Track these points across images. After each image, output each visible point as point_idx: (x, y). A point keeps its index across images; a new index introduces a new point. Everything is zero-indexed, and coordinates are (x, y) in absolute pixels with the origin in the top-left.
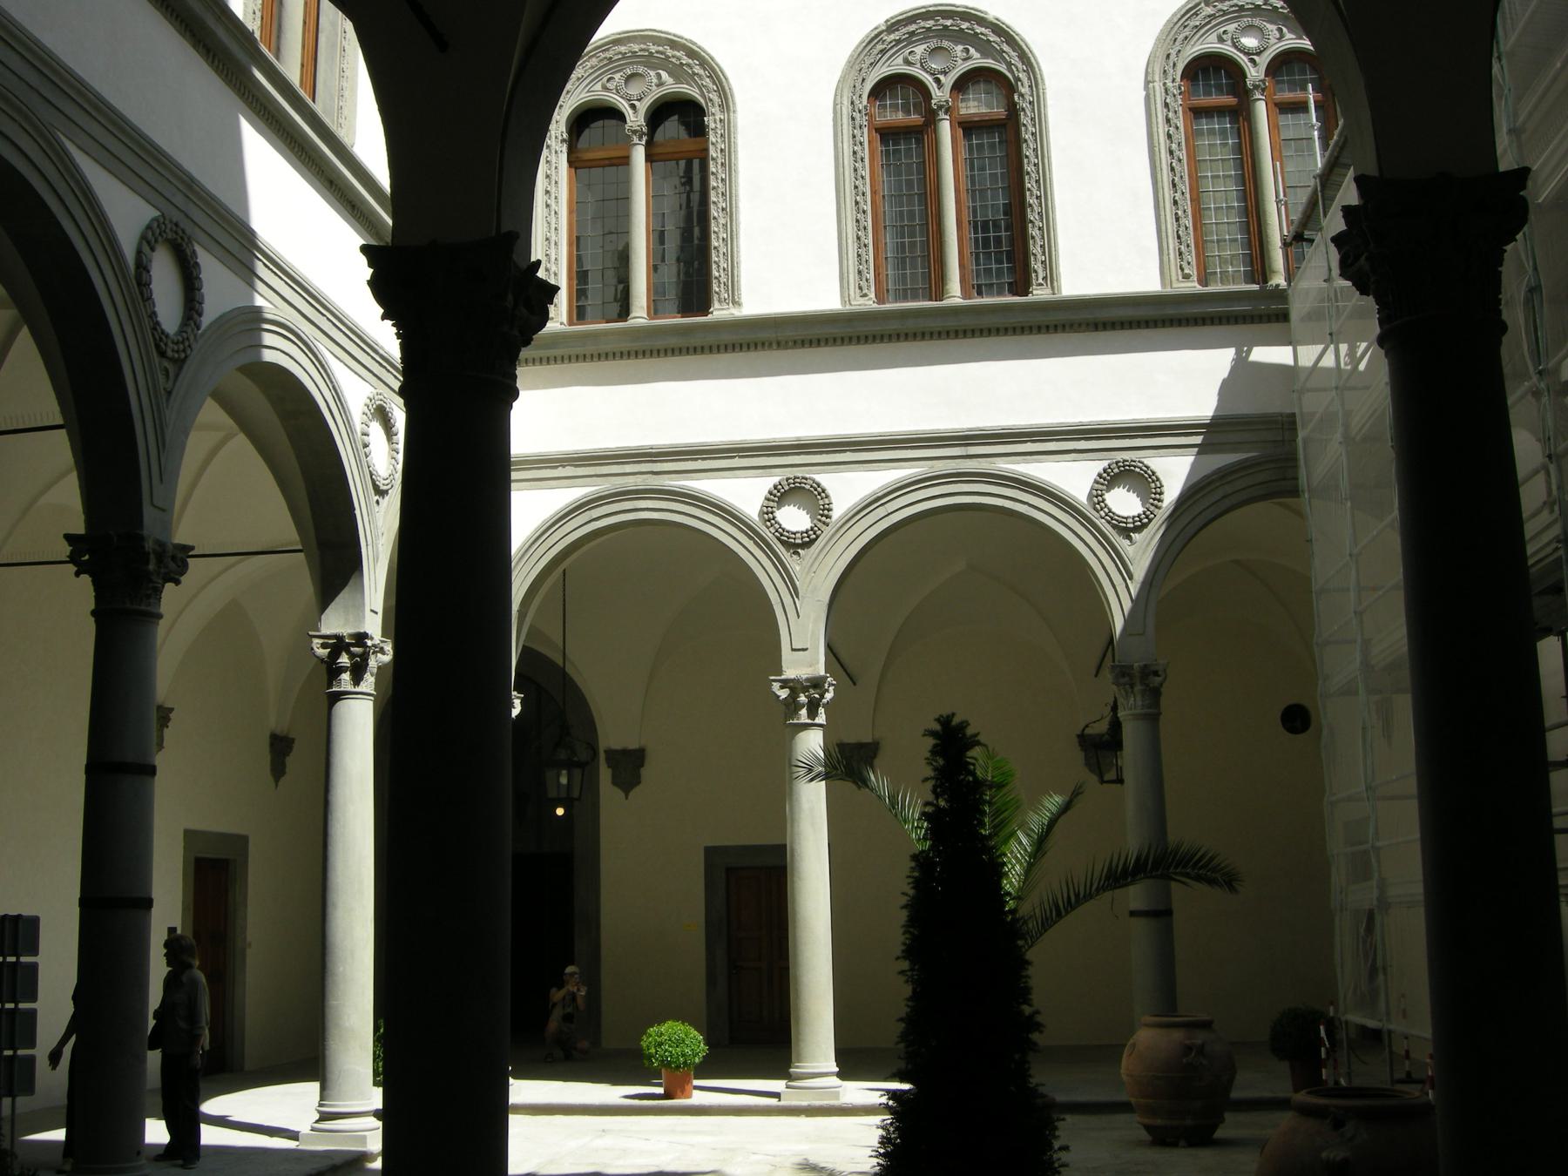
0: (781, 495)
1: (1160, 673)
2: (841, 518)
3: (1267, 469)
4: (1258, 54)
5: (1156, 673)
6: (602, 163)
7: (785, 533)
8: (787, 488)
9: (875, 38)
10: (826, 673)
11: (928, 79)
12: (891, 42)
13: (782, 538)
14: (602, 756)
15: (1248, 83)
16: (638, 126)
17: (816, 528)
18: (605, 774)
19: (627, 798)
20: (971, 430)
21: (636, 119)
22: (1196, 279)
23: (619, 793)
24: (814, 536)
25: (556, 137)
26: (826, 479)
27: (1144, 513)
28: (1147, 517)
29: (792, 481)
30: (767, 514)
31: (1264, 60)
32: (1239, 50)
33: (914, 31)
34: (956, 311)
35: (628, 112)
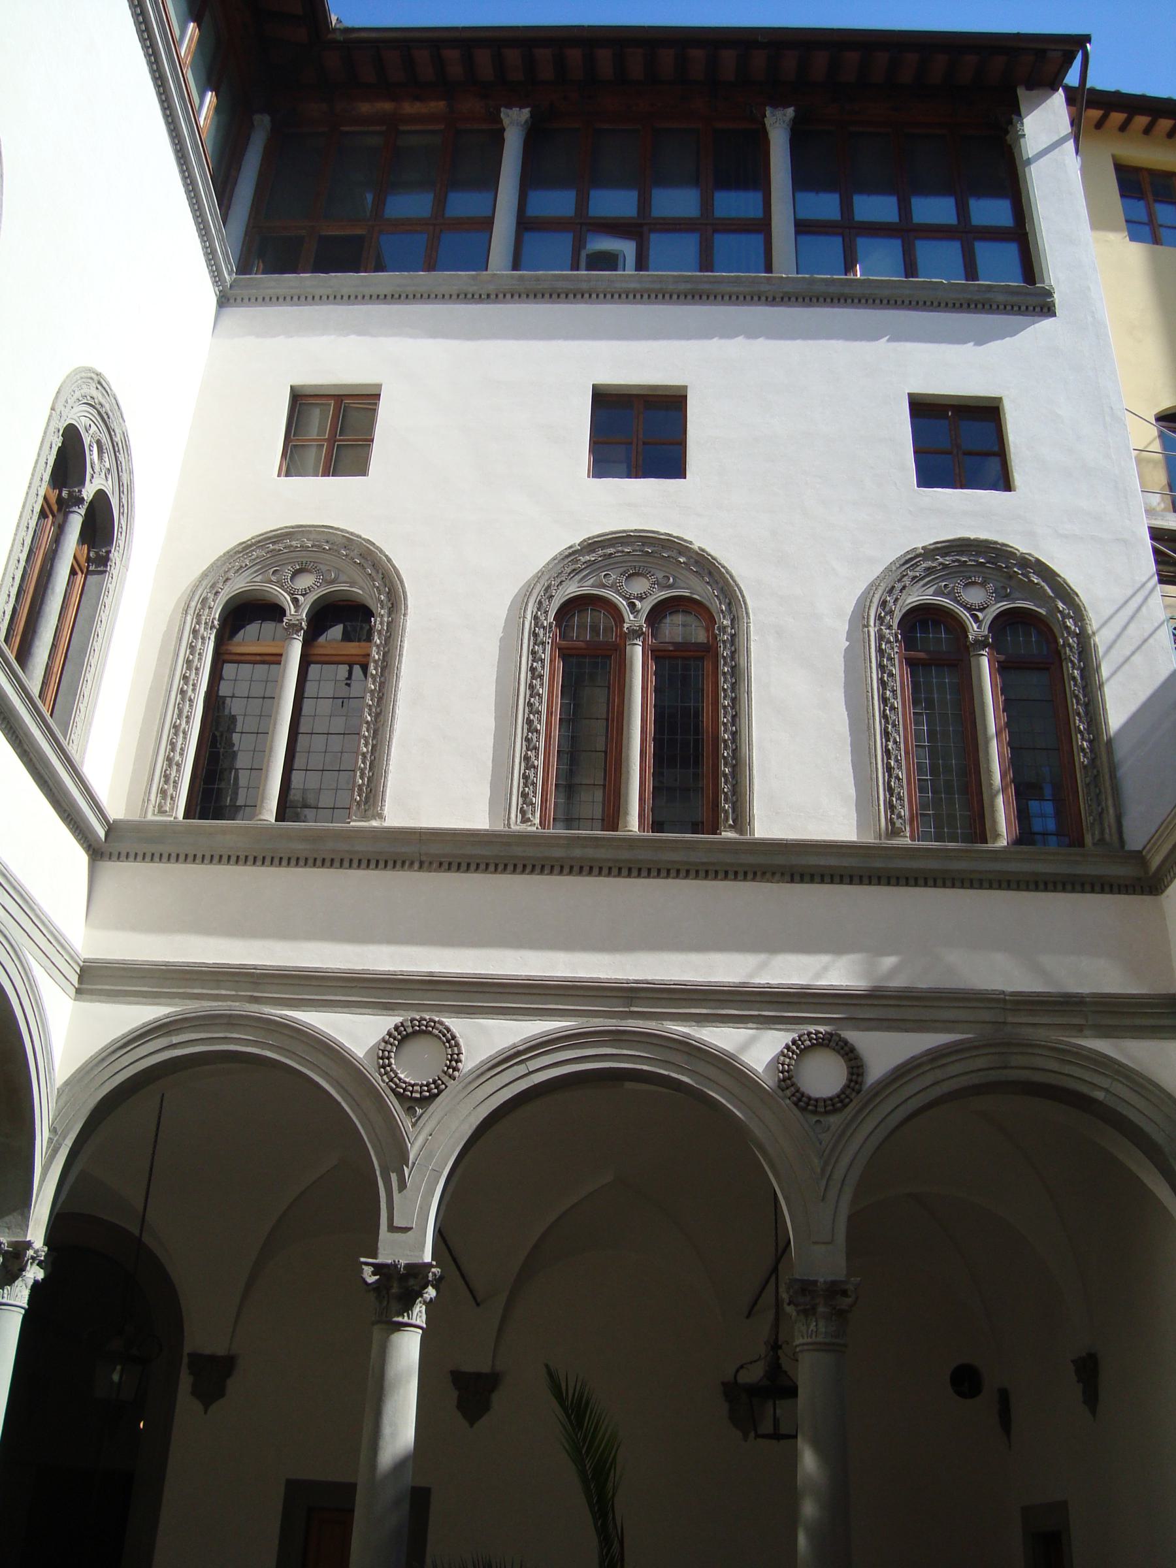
0: (402, 1037)
1: (849, 1293)
2: (471, 1072)
3: (993, 1054)
4: (981, 610)
5: (844, 1293)
6: (253, 658)
7: (395, 1079)
8: (410, 1030)
9: (572, 555)
10: (432, 1260)
11: (622, 604)
12: (585, 562)
13: (398, 1089)
14: (185, 1360)
15: (970, 637)
16: (298, 620)
17: (440, 1082)
18: (185, 1381)
19: (206, 1413)
20: (637, 982)
21: (297, 614)
22: (908, 835)
23: (197, 1406)
24: (436, 1091)
25: (206, 623)
26: (456, 1025)
27: (434, 1082)
28: (841, 1101)
29: (425, 1023)
30: (382, 1058)
31: (988, 617)
32: (961, 605)
33: (611, 554)
34: (632, 842)
35: (291, 609)
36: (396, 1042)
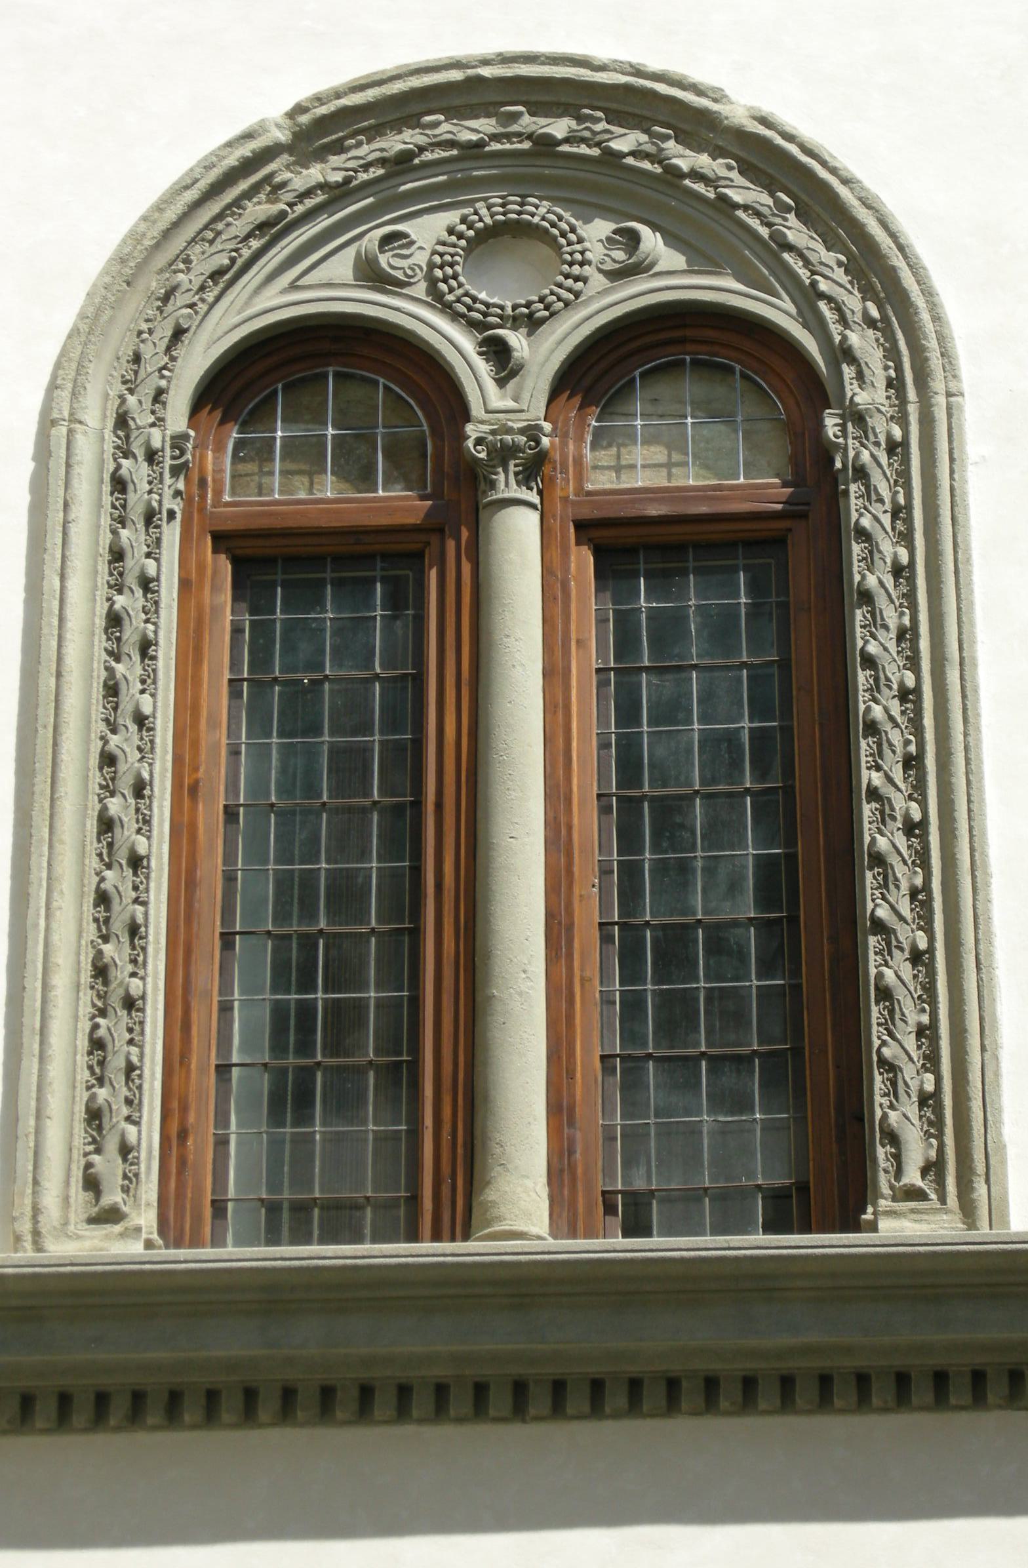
36: (463, 243)
